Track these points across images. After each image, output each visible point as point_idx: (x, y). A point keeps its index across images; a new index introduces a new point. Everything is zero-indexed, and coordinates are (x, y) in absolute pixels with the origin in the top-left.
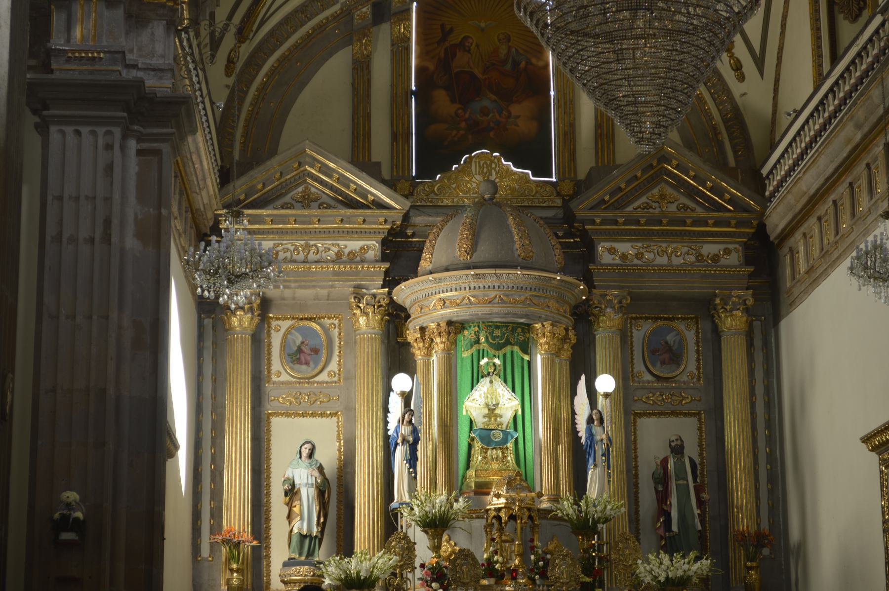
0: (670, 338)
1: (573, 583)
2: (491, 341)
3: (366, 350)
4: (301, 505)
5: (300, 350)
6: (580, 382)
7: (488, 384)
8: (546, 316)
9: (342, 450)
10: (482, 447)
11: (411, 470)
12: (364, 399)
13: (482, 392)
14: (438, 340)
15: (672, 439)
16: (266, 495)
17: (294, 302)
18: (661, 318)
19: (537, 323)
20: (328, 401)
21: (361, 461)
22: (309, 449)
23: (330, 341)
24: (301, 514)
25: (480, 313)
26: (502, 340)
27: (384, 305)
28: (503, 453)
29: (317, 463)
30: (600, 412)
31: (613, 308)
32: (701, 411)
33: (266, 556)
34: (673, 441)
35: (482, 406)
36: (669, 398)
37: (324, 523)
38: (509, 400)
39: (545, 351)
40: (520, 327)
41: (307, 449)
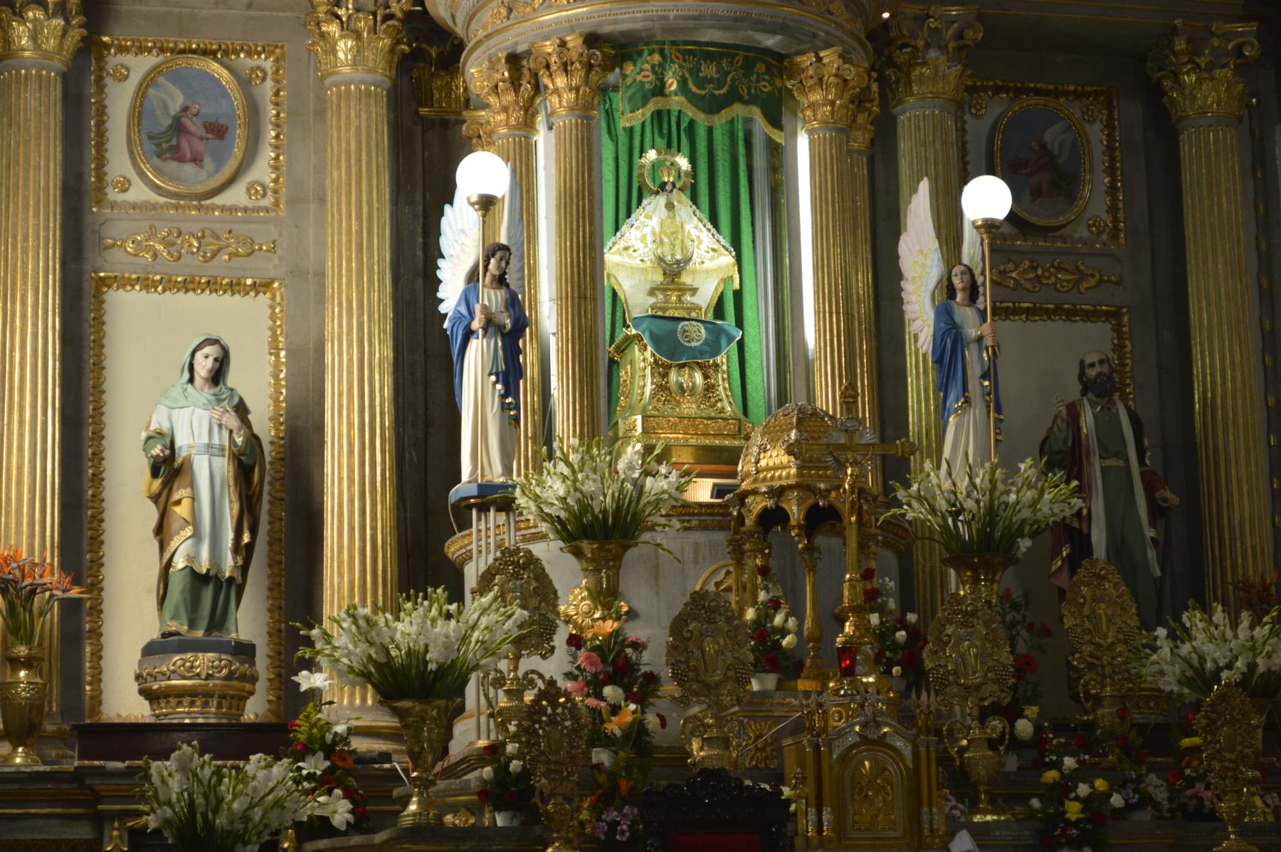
0: (1052, 136)
1: (992, 687)
2: (694, 89)
3: (354, 123)
4: (193, 499)
5: (178, 127)
6: (915, 199)
7: (663, 212)
8: (828, 33)
9: (282, 376)
10: (656, 362)
11: (509, 400)
12: (349, 241)
13: (647, 230)
14: (561, 81)
15: (1088, 360)
16: (92, 481)
17: (165, 9)
18: (1028, 91)
19: (803, 53)
20: (249, 254)
21: (340, 395)
22: (216, 360)
23: (254, 111)
24: (195, 522)
25: (672, 14)
26: (721, 88)
27: (399, 15)
28: (706, 377)
29: (231, 397)
30: (970, 271)
31: (943, 48)
32: (1121, 308)
33: (90, 631)
34: (1092, 365)
35: (648, 264)
36: (1051, 274)
37: (250, 547)
38: (712, 253)
39: (824, 122)
40: (762, 61)
41: (210, 360)
